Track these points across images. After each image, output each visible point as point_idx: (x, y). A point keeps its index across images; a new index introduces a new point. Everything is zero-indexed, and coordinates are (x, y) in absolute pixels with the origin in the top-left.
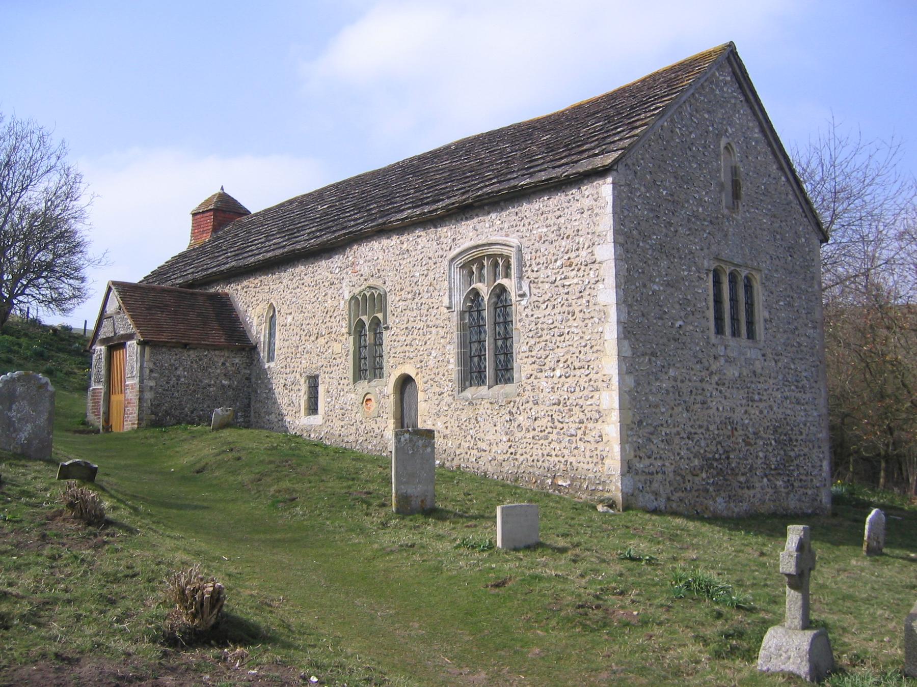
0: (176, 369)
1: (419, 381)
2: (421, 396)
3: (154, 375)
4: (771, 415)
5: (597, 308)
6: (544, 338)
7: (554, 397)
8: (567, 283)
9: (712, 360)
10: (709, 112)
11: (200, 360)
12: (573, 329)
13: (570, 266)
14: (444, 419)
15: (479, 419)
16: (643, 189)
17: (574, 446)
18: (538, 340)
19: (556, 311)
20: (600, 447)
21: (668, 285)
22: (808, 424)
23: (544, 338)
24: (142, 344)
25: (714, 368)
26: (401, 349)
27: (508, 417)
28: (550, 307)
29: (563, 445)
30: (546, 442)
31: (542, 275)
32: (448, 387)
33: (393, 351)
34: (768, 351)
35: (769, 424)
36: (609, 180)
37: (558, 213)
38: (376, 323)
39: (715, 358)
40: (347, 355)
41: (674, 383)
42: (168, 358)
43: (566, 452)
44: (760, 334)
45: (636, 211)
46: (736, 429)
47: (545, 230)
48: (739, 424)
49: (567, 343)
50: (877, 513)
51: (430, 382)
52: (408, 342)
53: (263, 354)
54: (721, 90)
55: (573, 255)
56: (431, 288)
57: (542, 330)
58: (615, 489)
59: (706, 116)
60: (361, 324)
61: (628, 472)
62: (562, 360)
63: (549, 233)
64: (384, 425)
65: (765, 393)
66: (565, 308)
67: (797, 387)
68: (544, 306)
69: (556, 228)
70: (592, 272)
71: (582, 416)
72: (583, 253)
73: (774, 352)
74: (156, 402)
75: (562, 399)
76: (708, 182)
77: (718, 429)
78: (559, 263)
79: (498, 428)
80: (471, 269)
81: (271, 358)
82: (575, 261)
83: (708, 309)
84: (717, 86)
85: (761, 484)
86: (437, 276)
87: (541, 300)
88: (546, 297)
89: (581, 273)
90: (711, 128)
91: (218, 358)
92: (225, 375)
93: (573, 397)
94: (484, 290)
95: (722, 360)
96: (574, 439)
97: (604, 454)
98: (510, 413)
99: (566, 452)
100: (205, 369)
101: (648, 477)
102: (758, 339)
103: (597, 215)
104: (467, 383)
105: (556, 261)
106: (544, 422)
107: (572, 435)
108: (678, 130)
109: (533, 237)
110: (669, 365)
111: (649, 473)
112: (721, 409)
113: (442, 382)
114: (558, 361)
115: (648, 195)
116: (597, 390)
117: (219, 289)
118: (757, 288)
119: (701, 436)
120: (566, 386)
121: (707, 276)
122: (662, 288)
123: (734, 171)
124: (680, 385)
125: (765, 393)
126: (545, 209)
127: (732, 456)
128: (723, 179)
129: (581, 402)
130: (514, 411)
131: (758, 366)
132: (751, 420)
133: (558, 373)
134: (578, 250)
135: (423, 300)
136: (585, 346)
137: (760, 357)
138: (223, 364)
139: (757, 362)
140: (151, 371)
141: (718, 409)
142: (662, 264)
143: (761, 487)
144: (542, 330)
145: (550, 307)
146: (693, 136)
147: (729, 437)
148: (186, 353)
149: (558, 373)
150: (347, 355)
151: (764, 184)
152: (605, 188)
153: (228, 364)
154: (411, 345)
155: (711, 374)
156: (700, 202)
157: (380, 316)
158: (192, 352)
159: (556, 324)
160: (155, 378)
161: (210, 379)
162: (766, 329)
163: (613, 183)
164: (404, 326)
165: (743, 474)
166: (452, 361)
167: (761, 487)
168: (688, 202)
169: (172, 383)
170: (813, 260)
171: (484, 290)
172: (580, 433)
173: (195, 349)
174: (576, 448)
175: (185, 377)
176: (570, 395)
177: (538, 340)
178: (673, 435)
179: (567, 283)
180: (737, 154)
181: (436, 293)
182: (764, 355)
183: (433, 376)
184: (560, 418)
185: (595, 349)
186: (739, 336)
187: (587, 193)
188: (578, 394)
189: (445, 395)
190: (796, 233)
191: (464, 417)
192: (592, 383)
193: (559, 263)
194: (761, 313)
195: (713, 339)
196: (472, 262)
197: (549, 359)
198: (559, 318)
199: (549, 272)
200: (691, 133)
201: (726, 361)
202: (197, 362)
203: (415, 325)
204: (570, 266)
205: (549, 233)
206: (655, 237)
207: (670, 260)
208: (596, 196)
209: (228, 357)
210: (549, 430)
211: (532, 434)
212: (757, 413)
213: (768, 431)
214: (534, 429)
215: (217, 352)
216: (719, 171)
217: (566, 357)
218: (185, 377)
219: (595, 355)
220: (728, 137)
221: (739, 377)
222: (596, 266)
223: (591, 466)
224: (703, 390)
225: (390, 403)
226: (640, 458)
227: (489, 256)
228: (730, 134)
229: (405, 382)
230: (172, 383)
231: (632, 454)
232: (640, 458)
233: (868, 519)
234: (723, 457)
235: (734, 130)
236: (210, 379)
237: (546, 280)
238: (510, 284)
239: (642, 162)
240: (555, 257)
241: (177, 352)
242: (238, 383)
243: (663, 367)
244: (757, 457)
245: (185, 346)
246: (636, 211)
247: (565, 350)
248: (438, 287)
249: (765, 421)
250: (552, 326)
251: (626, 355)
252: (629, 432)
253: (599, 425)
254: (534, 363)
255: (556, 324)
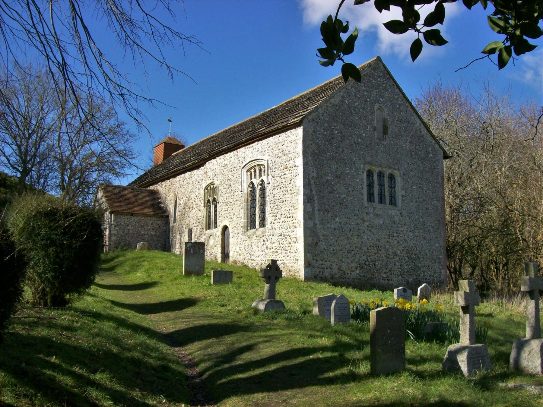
0: (128, 226)
1: (230, 228)
2: (231, 236)
3: (116, 228)
4: (405, 244)
5: (296, 188)
6: (276, 204)
7: (280, 232)
8: (285, 176)
9: (365, 215)
10: (367, 91)
11: (140, 222)
12: (288, 199)
13: (287, 168)
14: (239, 246)
15: (252, 245)
16: (322, 130)
17: (287, 255)
18: (274, 205)
19: (281, 190)
20: (296, 254)
21: (337, 176)
22: (432, 250)
23: (276, 204)
24: (111, 213)
25: (366, 218)
26: (224, 213)
27: (263, 243)
28: (279, 189)
29: (283, 255)
30: (276, 254)
31: (276, 173)
32: (241, 230)
33: (221, 214)
34: (404, 212)
35: (404, 249)
36: (302, 127)
37: (283, 143)
38: (214, 200)
39: (367, 213)
40: (203, 217)
41: (339, 225)
42: (124, 220)
43: (284, 258)
44: (399, 203)
45: (317, 141)
46: (380, 250)
47: (278, 151)
48: (382, 248)
49: (285, 206)
50: (425, 286)
51: (234, 228)
52: (226, 209)
53: (172, 219)
54: (376, 80)
55: (287, 163)
56: (235, 182)
57: (276, 200)
58: (301, 275)
59: (366, 93)
60: (209, 201)
61: (308, 266)
62: (283, 214)
63: (279, 153)
64: (217, 251)
65: (401, 233)
66: (285, 189)
67: (424, 231)
68: (277, 188)
69: (282, 150)
70: (295, 171)
71: (290, 241)
72: (292, 162)
73: (408, 212)
74: (117, 242)
75: (283, 233)
76: (365, 126)
77: (368, 249)
78: (282, 167)
79: (259, 249)
80: (251, 172)
81: (175, 222)
82: (289, 166)
83: (363, 189)
84: (373, 78)
85: (397, 279)
86: (237, 176)
87: (276, 185)
88: (278, 184)
89: (291, 172)
90: (368, 100)
91: (149, 221)
92: (153, 230)
93: (287, 231)
94: (256, 181)
95: (372, 215)
96: (287, 252)
97: (298, 258)
98: (264, 241)
99: (284, 258)
100: (142, 226)
101: (322, 270)
102: (397, 205)
103: (297, 143)
104: (249, 228)
105: (281, 166)
106: (276, 244)
107: (286, 250)
108: (347, 102)
109: (273, 155)
110: (336, 216)
111: (322, 268)
112: (370, 239)
113: (239, 228)
114: (282, 215)
115: (325, 133)
116: (296, 227)
117: (152, 188)
118: (399, 180)
119: (357, 252)
120: (284, 226)
121: (363, 173)
122: (332, 179)
123: (384, 120)
124: (343, 226)
125: (401, 233)
126: (278, 142)
127: (377, 264)
128: (376, 125)
129: (290, 234)
130: (265, 240)
131: (397, 219)
132: (391, 246)
133: (281, 220)
134: (290, 160)
135: (232, 188)
136: (292, 207)
137: (398, 214)
138: (152, 224)
139: (396, 217)
140: (115, 226)
141: (368, 239)
142: (333, 167)
143: (397, 280)
144: (276, 200)
145: (279, 189)
146: (357, 104)
147: (375, 254)
148: (132, 218)
149: (281, 220)
150: (203, 217)
151: (404, 127)
152: (299, 131)
153: (154, 224)
154: (227, 210)
155: (364, 221)
156: (360, 136)
157: (216, 197)
158: (136, 218)
159: (281, 197)
160: (117, 230)
161: (145, 231)
162: (403, 200)
163: (303, 128)
164: (225, 202)
165: (385, 273)
166: (243, 217)
167: (397, 280)
168: (351, 136)
169: (125, 233)
170: (438, 165)
171: (256, 181)
172: (289, 248)
173: (137, 216)
174: (288, 256)
175: (132, 230)
176: (286, 230)
177: (274, 205)
178: (338, 251)
179: (285, 176)
180: (386, 112)
181: (237, 185)
182: (401, 213)
183: (235, 225)
184: (282, 242)
185: (295, 208)
186: (374, 202)
187: (293, 133)
188: (289, 230)
189: (240, 234)
190: (426, 151)
191: (247, 244)
192: (294, 224)
193: (282, 167)
194: (399, 192)
195: (366, 204)
196: (251, 168)
197: (278, 214)
198: (282, 193)
199: (279, 172)
200: (355, 102)
201: (374, 215)
202: (138, 223)
203: (229, 200)
204: (287, 168)
205: (279, 153)
206: (329, 154)
207: (338, 165)
208: (296, 135)
209: (155, 221)
210: (278, 248)
211: (272, 250)
212: (396, 243)
213: (403, 252)
214: (273, 248)
215: (149, 218)
216: (373, 120)
217: (285, 212)
218: (132, 230)
219: (295, 211)
220: (380, 103)
221: (383, 224)
222: (296, 168)
223: (293, 264)
224: (358, 229)
225: (219, 239)
226: (317, 260)
227: (258, 165)
228: (381, 102)
229: (225, 228)
230: (125, 233)
231: (312, 258)
232: (317, 260)
233: (419, 289)
234: (371, 263)
235: (384, 100)
236: (145, 231)
237: (278, 176)
238: (264, 178)
239: (322, 117)
240: (281, 165)
241: (128, 218)
242: (160, 233)
243: (332, 217)
244: (395, 265)
245: (132, 214)
246: (317, 141)
247: (284, 209)
248: (238, 182)
249: (401, 246)
250: (280, 198)
251: (308, 210)
252: (310, 248)
253: (296, 244)
254: (273, 216)
255: (281, 197)
